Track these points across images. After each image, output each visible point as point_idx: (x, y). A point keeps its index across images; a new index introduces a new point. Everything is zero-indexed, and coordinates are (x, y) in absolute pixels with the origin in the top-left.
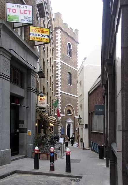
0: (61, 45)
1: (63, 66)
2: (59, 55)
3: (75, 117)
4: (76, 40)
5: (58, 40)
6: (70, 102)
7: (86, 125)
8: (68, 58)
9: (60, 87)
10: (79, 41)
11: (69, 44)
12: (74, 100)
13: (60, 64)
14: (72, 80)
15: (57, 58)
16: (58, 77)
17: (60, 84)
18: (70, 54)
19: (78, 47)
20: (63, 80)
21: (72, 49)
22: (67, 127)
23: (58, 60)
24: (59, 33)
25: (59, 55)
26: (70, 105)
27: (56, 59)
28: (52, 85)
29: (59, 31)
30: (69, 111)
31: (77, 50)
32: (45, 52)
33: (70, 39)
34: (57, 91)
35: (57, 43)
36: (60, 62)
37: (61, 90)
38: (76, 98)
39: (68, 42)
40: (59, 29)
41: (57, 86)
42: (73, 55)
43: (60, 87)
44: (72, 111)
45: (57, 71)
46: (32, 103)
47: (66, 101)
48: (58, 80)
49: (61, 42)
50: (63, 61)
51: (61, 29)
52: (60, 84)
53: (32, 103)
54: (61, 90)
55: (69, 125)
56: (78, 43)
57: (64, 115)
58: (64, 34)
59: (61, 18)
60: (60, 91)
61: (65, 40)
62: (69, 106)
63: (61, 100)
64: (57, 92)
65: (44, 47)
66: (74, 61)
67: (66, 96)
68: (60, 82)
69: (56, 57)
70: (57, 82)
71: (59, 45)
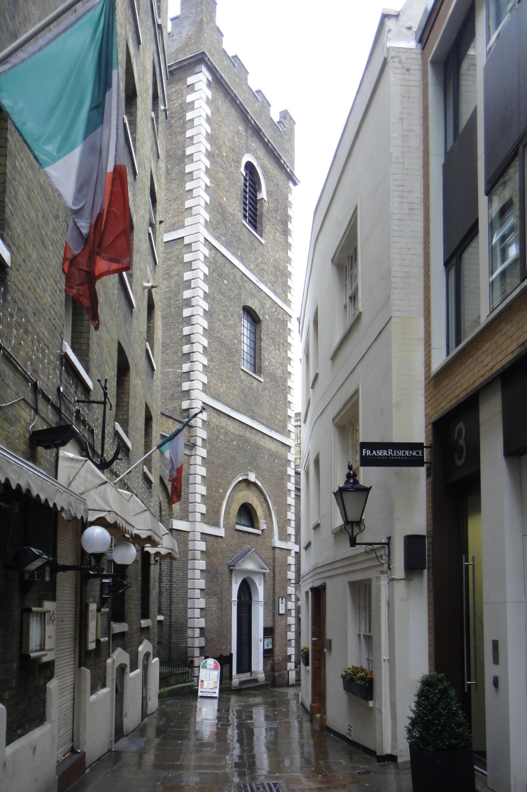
0: (210, 155)
1: (218, 266)
2: (200, 198)
3: (278, 543)
4: (284, 159)
5: (196, 105)
6: (252, 463)
7: (412, 542)
8: (246, 238)
9: (200, 378)
10: (298, 173)
11: (249, 166)
12: (274, 455)
13: (207, 252)
14: (265, 354)
15: (188, 221)
16: (194, 320)
17: (201, 359)
18: (253, 213)
19: (290, 198)
20: (221, 342)
21: (263, 194)
22: (235, 597)
23: (196, 230)
24: (200, 79)
25: (200, 198)
26: (252, 477)
27: (183, 227)
28: (204, 692)
29: (200, 79)
30: (247, 513)
31: (290, 212)
32: (153, 369)
33: (255, 144)
36: (203, 241)
37: (206, 388)
38: (282, 450)
39: (247, 158)
40: (204, 69)
41: (186, 367)
42: (268, 227)
43: (200, 378)
44: (260, 512)
45: (189, 287)
46: (475, 612)
47: (234, 458)
48: (194, 338)
49: (211, 138)
50: (217, 238)
51: (212, 70)
52: (201, 359)
53: (475, 612)
54: (206, 388)
55: (246, 589)
56: (291, 177)
57: (220, 532)
58: (225, 106)
59: (212, 18)
60: (200, 398)
61: (230, 136)
62: (247, 482)
63: (203, 447)
65: (152, 350)
66: (275, 260)
67: (232, 427)
68: (200, 367)
70: (186, 349)
71: (199, 150)
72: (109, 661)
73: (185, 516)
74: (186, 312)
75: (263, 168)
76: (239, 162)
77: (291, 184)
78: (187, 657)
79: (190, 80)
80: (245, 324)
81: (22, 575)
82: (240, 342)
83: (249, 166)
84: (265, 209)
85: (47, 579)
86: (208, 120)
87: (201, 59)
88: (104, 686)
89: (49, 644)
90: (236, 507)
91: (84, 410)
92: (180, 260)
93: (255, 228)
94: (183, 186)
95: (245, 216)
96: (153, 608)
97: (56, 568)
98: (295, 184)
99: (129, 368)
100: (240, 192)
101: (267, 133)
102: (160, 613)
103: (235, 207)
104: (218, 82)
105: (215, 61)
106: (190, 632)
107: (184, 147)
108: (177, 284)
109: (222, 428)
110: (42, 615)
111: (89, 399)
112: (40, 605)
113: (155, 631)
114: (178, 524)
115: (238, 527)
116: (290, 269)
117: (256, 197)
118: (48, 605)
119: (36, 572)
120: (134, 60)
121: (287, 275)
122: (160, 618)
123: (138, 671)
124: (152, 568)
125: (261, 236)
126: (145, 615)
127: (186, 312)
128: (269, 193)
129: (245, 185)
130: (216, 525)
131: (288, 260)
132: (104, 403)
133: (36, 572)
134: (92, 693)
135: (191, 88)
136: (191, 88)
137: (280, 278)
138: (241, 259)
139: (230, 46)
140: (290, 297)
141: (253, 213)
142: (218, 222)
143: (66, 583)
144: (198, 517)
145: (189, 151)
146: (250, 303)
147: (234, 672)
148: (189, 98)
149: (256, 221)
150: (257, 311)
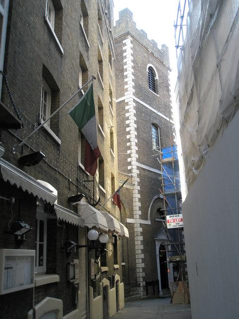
0: (133, 68)
1: (139, 109)
9: (135, 156)
13: (134, 104)
15: (126, 93)
19: (169, 77)
21: (157, 78)
23: (129, 97)
27: (124, 95)
31: (169, 82)
34: (130, 163)
35: (126, 62)
40: (129, 37)
41: (129, 152)
42: (160, 90)
49: (133, 61)
51: (132, 37)
59: (132, 19)
64: (129, 168)
69: (122, 91)
72: (101, 284)
73: (132, 217)
74: (128, 129)
75: (156, 68)
76: (146, 68)
77: (169, 71)
78: (137, 282)
79: (124, 42)
80: (153, 130)
81: (66, 251)
82: (152, 138)
83: (150, 68)
84: (158, 83)
85: (75, 251)
86: (132, 55)
87: (128, 34)
88: (99, 295)
89: (77, 277)
90: (155, 210)
91: (86, 184)
92: (123, 108)
93: (155, 91)
94: (123, 80)
95: (150, 87)
96: (119, 258)
97: (78, 247)
98: (171, 71)
99: (103, 161)
100: (147, 79)
101: (156, 55)
102: (123, 262)
103: (146, 85)
104: (135, 41)
105: (133, 34)
106: (137, 270)
107: (123, 66)
108: (123, 119)
109: (146, 176)
110: (74, 266)
111: (88, 179)
112: (73, 262)
113: (121, 270)
114: (129, 221)
115: (157, 219)
116: (171, 105)
117: (154, 79)
118: (76, 261)
119: (24, 235)
120: (101, 51)
121: (170, 107)
122: (123, 264)
123: (114, 289)
124: (118, 241)
125: (157, 94)
126: (116, 263)
127: (128, 129)
128: (160, 77)
129: (149, 75)
130: (146, 219)
131: (171, 102)
132: (94, 181)
133: (24, 235)
134: (94, 298)
135: (125, 45)
136: (125, 45)
137: (167, 109)
138: (149, 105)
139: (139, 27)
140: (172, 116)
141: (153, 85)
142: (139, 91)
143: (83, 251)
144: (138, 217)
145: (125, 67)
146: (155, 122)
147: (160, 289)
148: (124, 48)
149: (155, 88)
150: (158, 124)
